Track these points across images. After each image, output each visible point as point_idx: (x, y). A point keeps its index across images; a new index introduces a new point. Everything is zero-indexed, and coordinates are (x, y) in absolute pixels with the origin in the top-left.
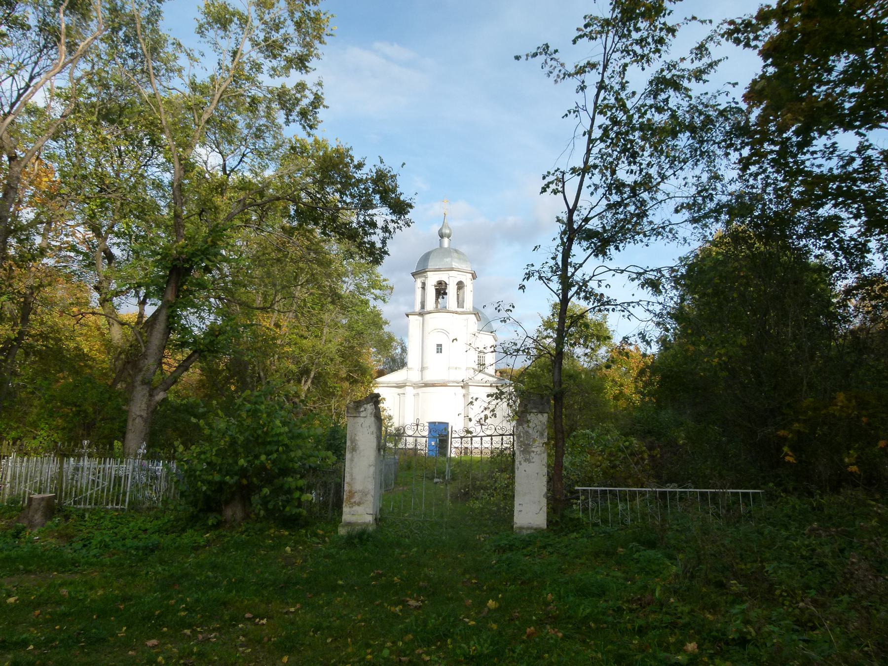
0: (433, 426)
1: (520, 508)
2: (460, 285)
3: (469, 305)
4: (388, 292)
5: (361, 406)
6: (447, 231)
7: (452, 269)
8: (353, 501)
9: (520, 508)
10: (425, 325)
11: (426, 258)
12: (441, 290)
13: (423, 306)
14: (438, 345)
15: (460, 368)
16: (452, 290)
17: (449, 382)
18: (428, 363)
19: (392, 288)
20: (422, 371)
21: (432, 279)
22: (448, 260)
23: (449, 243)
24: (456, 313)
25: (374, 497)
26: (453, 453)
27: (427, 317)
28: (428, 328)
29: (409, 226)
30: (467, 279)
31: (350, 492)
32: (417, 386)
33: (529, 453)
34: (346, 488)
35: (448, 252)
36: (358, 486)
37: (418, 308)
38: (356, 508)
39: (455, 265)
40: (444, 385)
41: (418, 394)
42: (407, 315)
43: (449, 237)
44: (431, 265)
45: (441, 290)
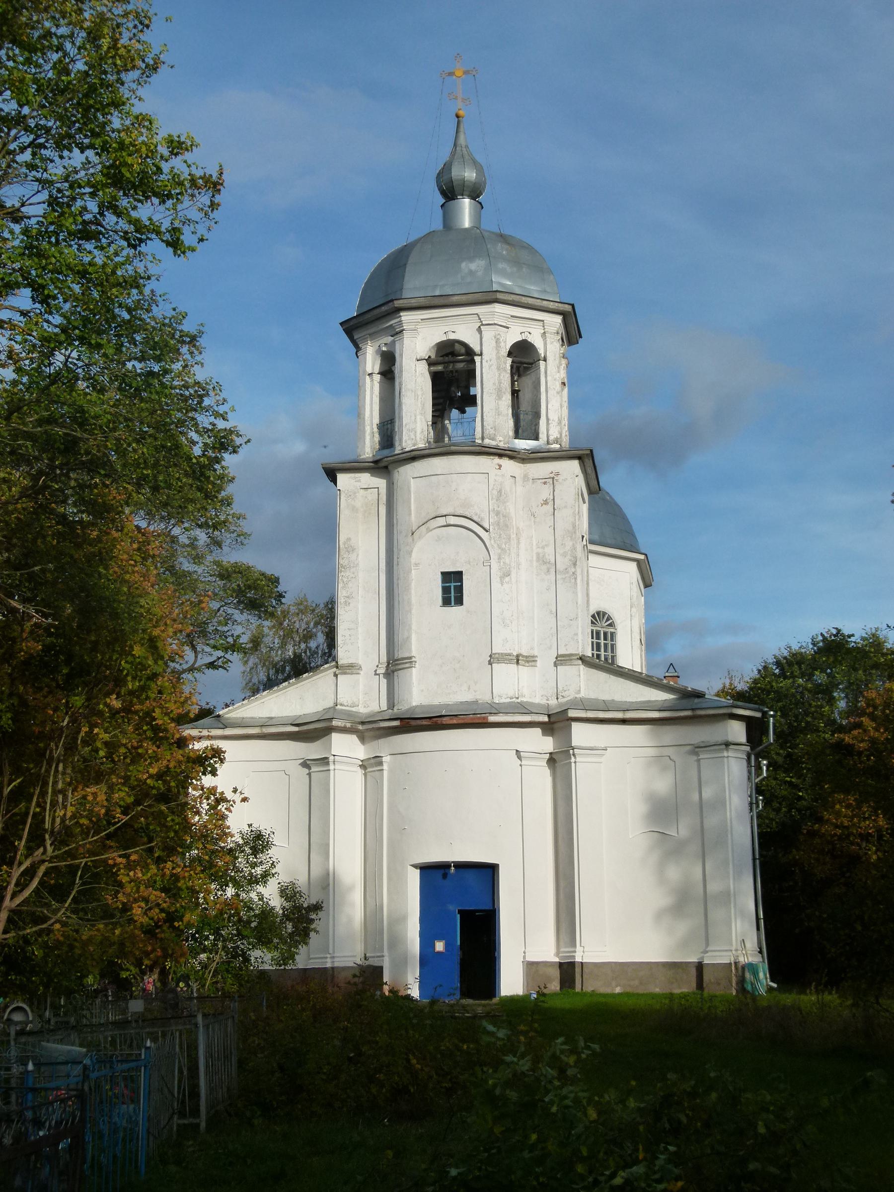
0: (434, 874)
2: (523, 358)
4: (190, 207)
6: (470, 175)
7: (490, 298)
10: (400, 510)
11: (394, 267)
12: (453, 377)
15: (530, 660)
16: (492, 378)
17: (497, 709)
19: (214, 185)
21: (420, 337)
22: (477, 265)
23: (477, 216)
24: (511, 454)
25: (409, 603)
26: (511, 982)
27: (407, 473)
30: (544, 333)
32: (371, 729)
35: (476, 242)
37: (369, 445)
39: (501, 282)
40: (472, 719)
41: (377, 761)
42: (331, 474)
43: (475, 193)
44: (414, 285)
45: (453, 377)
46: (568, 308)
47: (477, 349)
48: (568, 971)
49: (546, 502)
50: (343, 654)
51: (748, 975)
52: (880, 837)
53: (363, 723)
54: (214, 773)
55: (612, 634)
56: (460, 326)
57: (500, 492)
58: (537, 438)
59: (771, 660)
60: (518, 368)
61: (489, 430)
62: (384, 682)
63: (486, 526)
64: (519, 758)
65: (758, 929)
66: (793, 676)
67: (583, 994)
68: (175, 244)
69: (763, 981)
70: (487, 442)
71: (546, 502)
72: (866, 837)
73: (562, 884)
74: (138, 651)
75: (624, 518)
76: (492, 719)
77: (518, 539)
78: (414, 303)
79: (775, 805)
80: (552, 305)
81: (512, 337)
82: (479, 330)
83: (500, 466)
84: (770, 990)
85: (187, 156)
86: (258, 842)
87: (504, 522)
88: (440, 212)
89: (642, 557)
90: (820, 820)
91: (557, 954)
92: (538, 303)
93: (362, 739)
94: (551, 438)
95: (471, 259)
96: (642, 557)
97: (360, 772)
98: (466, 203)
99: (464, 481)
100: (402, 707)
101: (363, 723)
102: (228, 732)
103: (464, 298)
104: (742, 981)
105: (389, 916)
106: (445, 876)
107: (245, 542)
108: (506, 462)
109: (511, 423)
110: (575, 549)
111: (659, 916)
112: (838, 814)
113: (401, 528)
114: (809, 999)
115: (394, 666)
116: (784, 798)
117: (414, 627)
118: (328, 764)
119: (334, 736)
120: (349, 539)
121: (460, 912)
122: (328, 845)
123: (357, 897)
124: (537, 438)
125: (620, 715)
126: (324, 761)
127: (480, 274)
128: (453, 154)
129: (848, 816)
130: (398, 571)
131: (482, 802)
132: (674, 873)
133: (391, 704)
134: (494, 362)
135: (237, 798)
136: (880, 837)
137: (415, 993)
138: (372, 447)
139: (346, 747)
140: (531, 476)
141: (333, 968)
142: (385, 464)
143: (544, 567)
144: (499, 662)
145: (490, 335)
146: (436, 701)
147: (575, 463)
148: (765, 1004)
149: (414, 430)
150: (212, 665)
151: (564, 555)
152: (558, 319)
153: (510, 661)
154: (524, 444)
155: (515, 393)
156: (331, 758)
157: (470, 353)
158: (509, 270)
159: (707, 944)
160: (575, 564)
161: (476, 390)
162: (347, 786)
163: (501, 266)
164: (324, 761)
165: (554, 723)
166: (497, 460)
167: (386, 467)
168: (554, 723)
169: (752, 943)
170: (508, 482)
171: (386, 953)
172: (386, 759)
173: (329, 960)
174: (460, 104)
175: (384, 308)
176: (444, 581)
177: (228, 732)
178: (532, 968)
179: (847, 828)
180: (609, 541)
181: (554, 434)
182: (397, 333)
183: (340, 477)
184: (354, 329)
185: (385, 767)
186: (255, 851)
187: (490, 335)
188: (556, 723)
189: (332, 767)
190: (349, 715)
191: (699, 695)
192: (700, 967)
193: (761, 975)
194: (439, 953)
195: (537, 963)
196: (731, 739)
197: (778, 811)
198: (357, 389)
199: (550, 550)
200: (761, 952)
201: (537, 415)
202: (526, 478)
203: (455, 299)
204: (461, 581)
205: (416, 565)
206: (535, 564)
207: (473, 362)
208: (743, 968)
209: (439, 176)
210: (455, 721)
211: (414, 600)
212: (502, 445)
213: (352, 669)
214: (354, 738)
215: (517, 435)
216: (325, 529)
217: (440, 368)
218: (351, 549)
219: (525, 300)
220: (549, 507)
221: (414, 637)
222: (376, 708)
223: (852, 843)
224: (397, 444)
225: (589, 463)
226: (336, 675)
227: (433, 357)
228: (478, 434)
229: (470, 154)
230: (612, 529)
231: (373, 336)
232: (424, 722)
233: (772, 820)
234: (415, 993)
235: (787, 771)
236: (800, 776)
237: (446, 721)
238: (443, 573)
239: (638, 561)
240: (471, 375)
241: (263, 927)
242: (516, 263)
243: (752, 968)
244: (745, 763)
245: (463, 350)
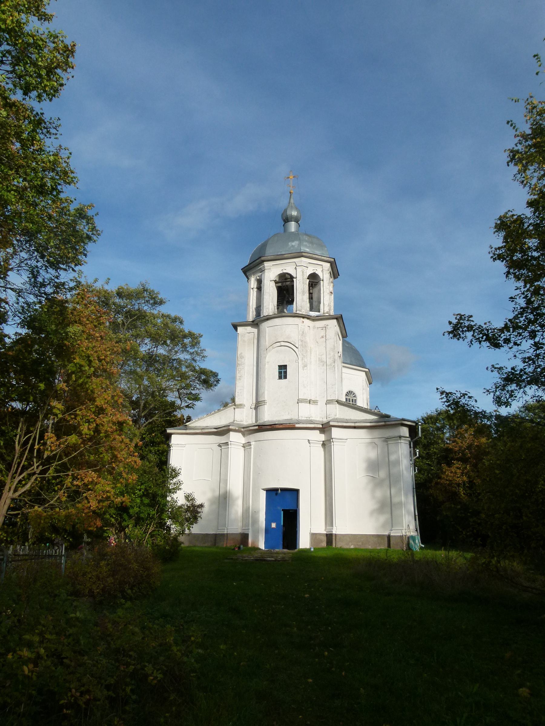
0: (272, 493)
2: (314, 281)
3: (327, 303)
6: (294, 213)
7: (300, 255)
11: (263, 247)
12: (285, 291)
13: (259, 309)
14: (281, 367)
15: (315, 402)
18: (266, 396)
20: (256, 408)
21: (272, 272)
22: (295, 243)
26: (304, 542)
27: (265, 326)
28: (267, 340)
30: (323, 270)
37: (251, 316)
40: (289, 426)
41: (249, 444)
42: (235, 327)
43: (297, 220)
44: (270, 252)
45: (285, 291)
46: (333, 260)
47: (295, 276)
48: (330, 537)
49: (323, 337)
51: (411, 542)
52: (464, 484)
53: (243, 428)
55: (355, 400)
56: (287, 267)
57: (303, 332)
58: (319, 312)
59: (420, 418)
60: (312, 284)
61: (299, 308)
63: (297, 346)
64: (309, 443)
65: (415, 520)
66: (428, 423)
67: (336, 548)
69: (417, 545)
70: (298, 312)
71: (323, 337)
72: (459, 485)
73: (328, 498)
75: (360, 355)
76: (297, 426)
77: (311, 352)
78: (269, 258)
79: (422, 472)
80: (325, 258)
81: (310, 271)
82: (296, 268)
83: (303, 322)
84: (421, 548)
87: (304, 345)
88: (283, 227)
89: (367, 370)
90: (440, 478)
91: (325, 530)
93: (244, 435)
94: (325, 311)
95: (293, 241)
96: (367, 370)
97: (243, 449)
99: (287, 328)
100: (260, 422)
101: (243, 428)
102: (188, 431)
104: (408, 544)
105: (252, 511)
106: (276, 494)
107: (205, 359)
108: (305, 320)
109: (308, 305)
110: (335, 356)
111: (372, 513)
112: (447, 476)
113: (262, 348)
114: (441, 554)
115: (258, 404)
116: (426, 470)
117: (266, 388)
118: (228, 445)
119: (231, 433)
120: (242, 353)
121: (283, 510)
122: (227, 480)
123: (240, 502)
124: (319, 312)
125: (353, 425)
126: (227, 444)
127: (296, 246)
129: (455, 474)
131: (294, 462)
132: (379, 493)
133: (256, 421)
134: (301, 280)
136: (464, 484)
137: (262, 545)
138: (253, 317)
139: (235, 438)
140: (317, 326)
141: (227, 534)
142: (257, 322)
143: (322, 364)
145: (300, 270)
147: (335, 320)
148: (419, 556)
149: (268, 308)
150: (187, 406)
151: (330, 358)
152: (329, 265)
154: (313, 314)
155: (310, 294)
156: (229, 443)
157: (292, 277)
158: (308, 245)
159: (392, 527)
160: (334, 362)
163: (305, 243)
164: (227, 444)
165: (325, 428)
166: (302, 319)
167: (257, 324)
168: (325, 428)
169: (412, 526)
170: (307, 329)
171: (250, 528)
172: (253, 443)
173: (226, 530)
174: (291, 188)
175: (257, 261)
176: (279, 369)
177: (188, 431)
178: (314, 536)
179: (451, 481)
180: (354, 364)
181: (326, 310)
182: (262, 271)
183: (239, 329)
184: (247, 271)
185: (252, 446)
187: (300, 270)
188: (325, 428)
189: (230, 446)
191: (388, 416)
192: (389, 537)
193: (417, 541)
194: (273, 528)
195: (316, 534)
196: (402, 435)
197: (423, 474)
198: (247, 295)
199: (324, 356)
200: (417, 530)
201: (320, 303)
202: (314, 327)
204: (286, 369)
205: (268, 362)
206: (318, 362)
207: (293, 281)
208: (408, 538)
209: (282, 214)
210: (281, 427)
211: (266, 377)
212: (304, 313)
213: (241, 406)
214: (240, 435)
217: (280, 284)
218: (242, 357)
219: (314, 256)
220: (324, 339)
221: (266, 392)
222: (251, 423)
223: (453, 487)
224: (261, 314)
226: (234, 409)
227: (277, 280)
230: (353, 356)
231: (254, 274)
232: (268, 427)
233: (421, 478)
234: (262, 545)
235: (427, 459)
236: (432, 461)
237: (277, 426)
238: (279, 366)
241: (177, 514)
242: (312, 243)
243: (413, 538)
244: (409, 447)
245: (289, 277)
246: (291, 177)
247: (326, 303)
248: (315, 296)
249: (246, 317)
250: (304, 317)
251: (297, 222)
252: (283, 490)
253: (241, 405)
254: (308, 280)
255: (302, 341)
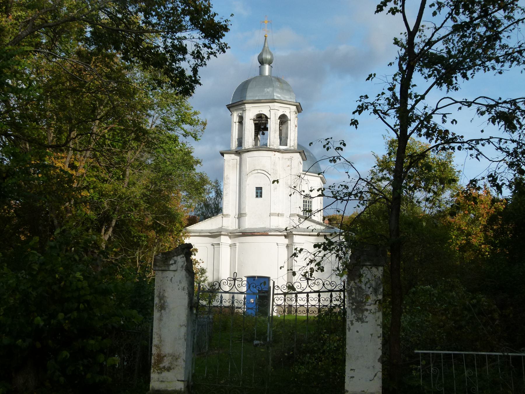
0: (251, 279)
1: (352, 374)
2: (283, 119)
3: (293, 140)
4: (199, 128)
5: (170, 259)
6: (268, 57)
7: (273, 101)
8: (161, 365)
9: (352, 374)
11: (243, 88)
12: (261, 125)
13: (240, 142)
15: (282, 215)
16: (273, 125)
17: (271, 230)
18: (247, 209)
19: (205, 124)
21: (251, 112)
22: (269, 90)
23: (270, 71)
24: (279, 151)
27: (246, 156)
29: (224, 52)
30: (290, 111)
31: (159, 355)
32: (233, 235)
33: (362, 311)
34: (154, 351)
35: (269, 81)
36: (167, 349)
37: (234, 145)
38: (165, 374)
40: (264, 233)
41: (235, 245)
42: (222, 154)
43: (270, 63)
44: (250, 95)
45: (261, 125)
46: (298, 104)
47: (269, 117)
49: (289, 166)
50: (225, 211)
54: (195, 255)
56: (263, 109)
58: (287, 145)
61: (272, 143)
62: (237, 220)
68: (195, 138)
70: (271, 147)
71: (289, 166)
74: (178, 225)
76: (270, 233)
78: (250, 101)
80: (293, 103)
81: (280, 113)
82: (270, 111)
85: (198, 116)
86: (203, 271)
92: (289, 103)
93: (230, 237)
95: (268, 88)
97: (229, 247)
98: (267, 67)
103: (265, 101)
106: (254, 280)
108: (276, 153)
109: (279, 140)
113: (243, 173)
115: (240, 215)
124: (287, 145)
126: (219, 244)
128: (263, 50)
130: (242, 192)
133: (239, 227)
134: (274, 121)
135: (201, 262)
139: (225, 240)
144: (272, 215)
145: (273, 112)
146: (253, 227)
149: (248, 142)
152: (295, 107)
153: (276, 215)
157: (267, 117)
161: (268, 126)
162: (225, 251)
164: (219, 244)
172: (237, 244)
181: (292, 144)
182: (244, 111)
183: (225, 155)
184: (230, 107)
185: (237, 246)
186: (202, 274)
190: (226, 230)
201: (287, 138)
202: (283, 158)
203: (262, 101)
211: (247, 196)
212: (275, 148)
213: (227, 216)
215: (280, 145)
216: (220, 171)
217: (257, 122)
218: (228, 178)
219: (284, 102)
221: (247, 207)
225: (303, 154)
228: (268, 144)
229: (269, 50)
231: (236, 110)
237: (256, 234)
239: (321, 177)
240: (266, 123)
242: (282, 89)
246: (266, 22)
247: (292, 138)
248: (284, 131)
249: (230, 145)
250: (275, 150)
251: (269, 65)
252: (259, 277)
253: (227, 215)
254: (279, 121)
255: (274, 169)
